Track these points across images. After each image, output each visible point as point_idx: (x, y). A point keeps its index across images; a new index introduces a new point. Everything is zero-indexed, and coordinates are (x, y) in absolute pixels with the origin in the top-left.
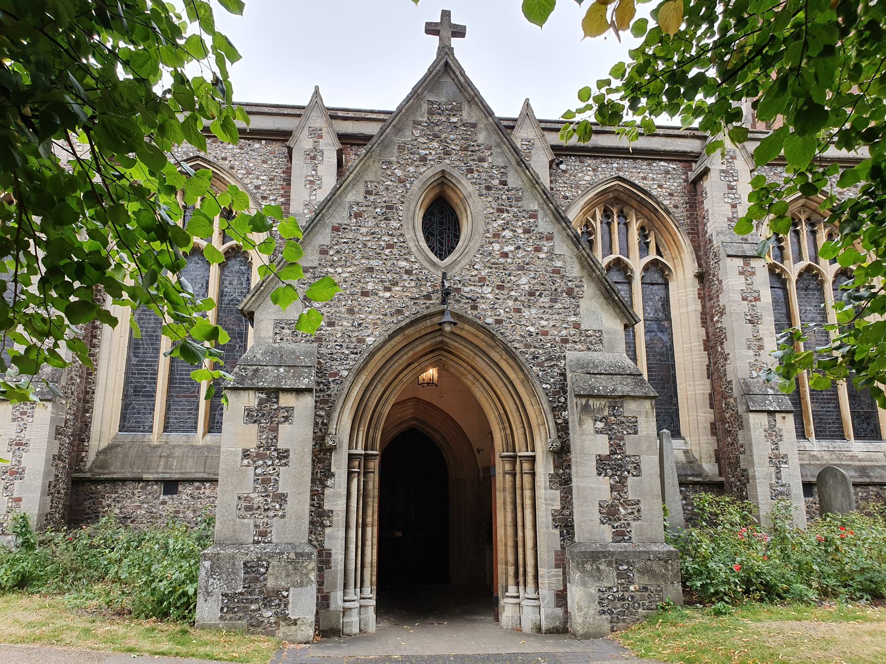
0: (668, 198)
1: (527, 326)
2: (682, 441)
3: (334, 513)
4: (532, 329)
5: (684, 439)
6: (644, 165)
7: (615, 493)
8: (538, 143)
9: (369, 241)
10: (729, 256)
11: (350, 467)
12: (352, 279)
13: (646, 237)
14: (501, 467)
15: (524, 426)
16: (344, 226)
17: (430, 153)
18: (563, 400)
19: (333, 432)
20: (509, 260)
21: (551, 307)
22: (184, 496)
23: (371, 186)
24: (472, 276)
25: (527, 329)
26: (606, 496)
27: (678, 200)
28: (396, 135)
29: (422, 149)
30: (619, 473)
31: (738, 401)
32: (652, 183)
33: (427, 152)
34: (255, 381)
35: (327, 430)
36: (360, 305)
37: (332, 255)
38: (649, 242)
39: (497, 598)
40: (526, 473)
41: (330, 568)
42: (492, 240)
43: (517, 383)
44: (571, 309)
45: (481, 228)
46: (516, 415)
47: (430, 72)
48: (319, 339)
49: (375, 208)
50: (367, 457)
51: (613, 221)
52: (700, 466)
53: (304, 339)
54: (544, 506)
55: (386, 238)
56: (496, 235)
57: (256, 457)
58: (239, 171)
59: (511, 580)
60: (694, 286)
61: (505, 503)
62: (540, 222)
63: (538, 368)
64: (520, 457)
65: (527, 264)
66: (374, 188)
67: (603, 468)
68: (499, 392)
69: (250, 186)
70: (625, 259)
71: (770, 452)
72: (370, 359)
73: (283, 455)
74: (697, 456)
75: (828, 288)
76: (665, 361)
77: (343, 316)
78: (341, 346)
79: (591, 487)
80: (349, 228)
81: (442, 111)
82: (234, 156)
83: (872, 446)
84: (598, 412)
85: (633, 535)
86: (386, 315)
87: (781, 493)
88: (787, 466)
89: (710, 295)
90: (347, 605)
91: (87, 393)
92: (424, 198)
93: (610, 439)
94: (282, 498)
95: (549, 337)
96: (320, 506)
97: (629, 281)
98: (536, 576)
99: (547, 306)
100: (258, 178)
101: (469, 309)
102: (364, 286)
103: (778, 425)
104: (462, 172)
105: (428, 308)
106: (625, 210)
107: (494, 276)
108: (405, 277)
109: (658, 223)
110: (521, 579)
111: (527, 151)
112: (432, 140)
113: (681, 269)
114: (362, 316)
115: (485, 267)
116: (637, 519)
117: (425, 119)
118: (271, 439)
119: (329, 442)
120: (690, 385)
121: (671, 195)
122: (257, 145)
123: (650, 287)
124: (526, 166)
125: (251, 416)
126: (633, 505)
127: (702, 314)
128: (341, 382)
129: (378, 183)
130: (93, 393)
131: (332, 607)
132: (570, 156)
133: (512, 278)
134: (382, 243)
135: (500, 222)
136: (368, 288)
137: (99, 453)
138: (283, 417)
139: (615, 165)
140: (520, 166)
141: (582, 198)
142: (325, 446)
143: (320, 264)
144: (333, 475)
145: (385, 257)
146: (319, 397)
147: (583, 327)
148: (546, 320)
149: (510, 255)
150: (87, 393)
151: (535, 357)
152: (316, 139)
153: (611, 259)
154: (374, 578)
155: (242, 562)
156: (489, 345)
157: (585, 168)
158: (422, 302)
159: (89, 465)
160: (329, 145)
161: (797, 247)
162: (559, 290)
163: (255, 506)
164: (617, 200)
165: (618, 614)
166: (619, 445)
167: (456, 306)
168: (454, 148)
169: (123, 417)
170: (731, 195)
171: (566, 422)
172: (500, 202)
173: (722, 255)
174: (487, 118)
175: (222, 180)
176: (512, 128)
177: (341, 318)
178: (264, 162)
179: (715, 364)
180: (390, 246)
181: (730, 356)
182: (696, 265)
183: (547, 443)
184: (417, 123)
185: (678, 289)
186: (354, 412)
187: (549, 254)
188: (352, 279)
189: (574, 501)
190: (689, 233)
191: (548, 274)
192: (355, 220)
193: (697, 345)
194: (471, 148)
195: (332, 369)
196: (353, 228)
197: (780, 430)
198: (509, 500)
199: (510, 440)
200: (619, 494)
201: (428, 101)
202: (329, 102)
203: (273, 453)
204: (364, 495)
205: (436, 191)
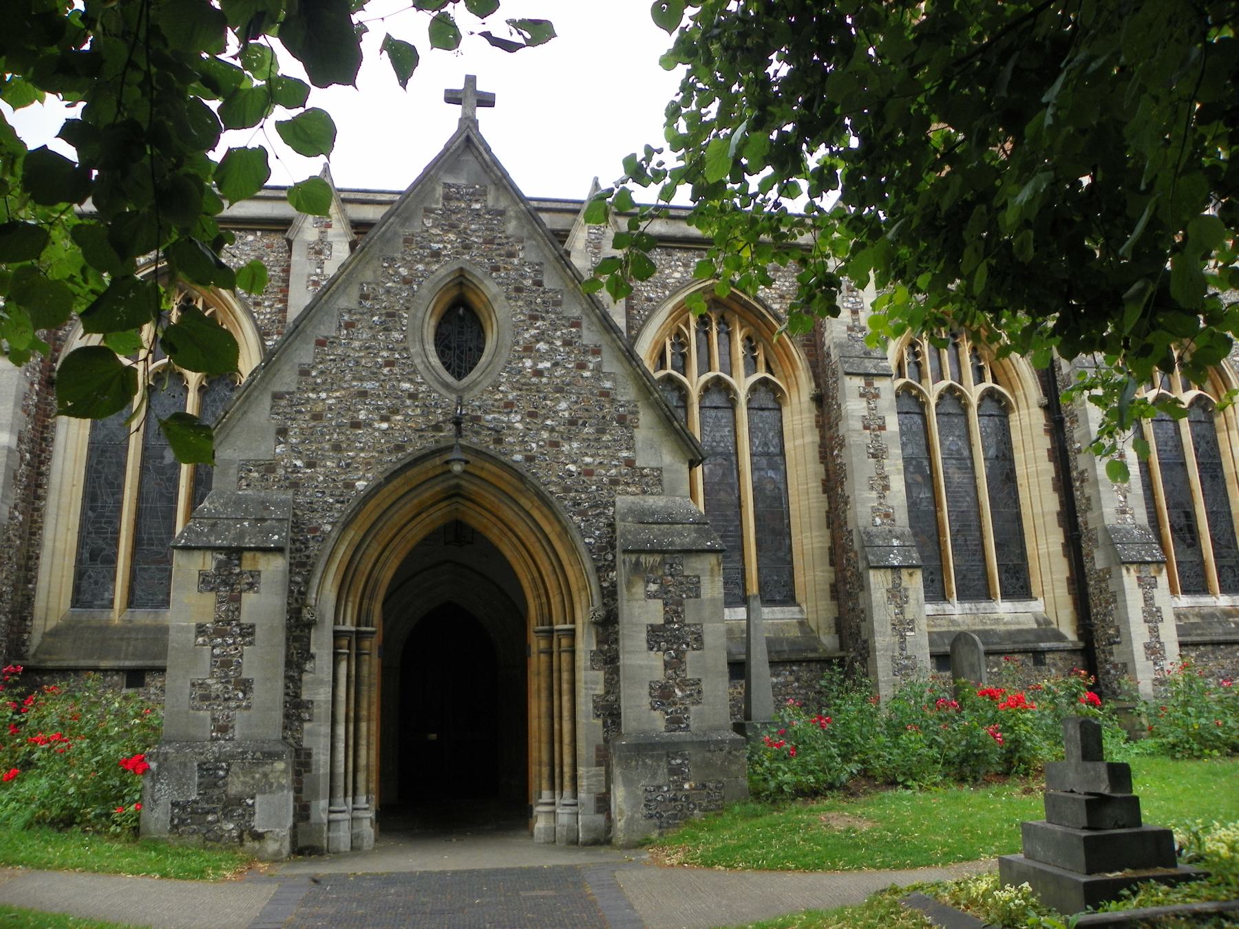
2: (796, 609)
4: (572, 467)
5: (799, 605)
7: (670, 672)
9: (362, 357)
10: (847, 374)
13: (753, 349)
14: (537, 644)
15: (561, 593)
17: (445, 248)
18: (610, 557)
20: (544, 380)
22: (152, 690)
24: (496, 400)
26: (659, 675)
28: (403, 225)
29: (435, 243)
30: (675, 647)
31: (859, 555)
33: (441, 246)
35: (304, 600)
37: (315, 377)
39: (531, 806)
41: (310, 771)
42: (522, 355)
43: (553, 537)
45: (508, 340)
46: (553, 577)
48: (295, 485)
50: (360, 636)
51: (711, 329)
52: (818, 639)
55: (385, 354)
56: (528, 349)
57: (214, 633)
59: (545, 784)
60: (810, 411)
62: (585, 332)
64: (558, 631)
65: (568, 385)
67: (656, 642)
68: (531, 548)
70: (727, 377)
71: (894, 617)
72: (360, 511)
74: (814, 627)
75: (973, 413)
77: (327, 454)
80: (337, 341)
83: (1020, 606)
85: (692, 722)
86: (382, 452)
87: (906, 667)
88: (913, 634)
89: (829, 423)
90: (333, 816)
91: (30, 558)
92: (437, 302)
93: (666, 605)
94: (245, 686)
95: (594, 478)
98: (574, 778)
102: (355, 415)
103: (903, 584)
105: (436, 442)
106: (726, 315)
108: (408, 402)
109: (766, 331)
110: (557, 781)
112: (448, 231)
113: (796, 389)
115: (513, 388)
120: (806, 537)
121: (782, 297)
122: (250, 238)
123: (760, 413)
125: (205, 582)
126: (693, 685)
127: (820, 446)
129: (378, 284)
130: (38, 558)
131: (313, 819)
133: (548, 402)
134: (379, 360)
135: (533, 332)
137: (45, 635)
138: (247, 584)
140: (560, 263)
143: (299, 388)
144: (312, 657)
145: (383, 377)
149: (546, 374)
150: (30, 558)
154: (373, 786)
155: (196, 764)
156: (517, 489)
159: (32, 650)
160: (340, 235)
161: (936, 363)
163: (213, 695)
165: (668, 817)
166: (676, 612)
167: (475, 440)
169: (77, 590)
170: (851, 299)
171: (614, 585)
172: (533, 307)
173: (840, 374)
177: (324, 458)
179: (836, 509)
180: (389, 363)
181: (851, 499)
182: (813, 385)
183: (588, 612)
184: (429, 211)
186: (342, 574)
187: (595, 372)
190: (804, 345)
193: (815, 486)
194: (498, 241)
195: (311, 523)
197: (906, 589)
198: (544, 685)
199: (546, 611)
204: (356, 682)
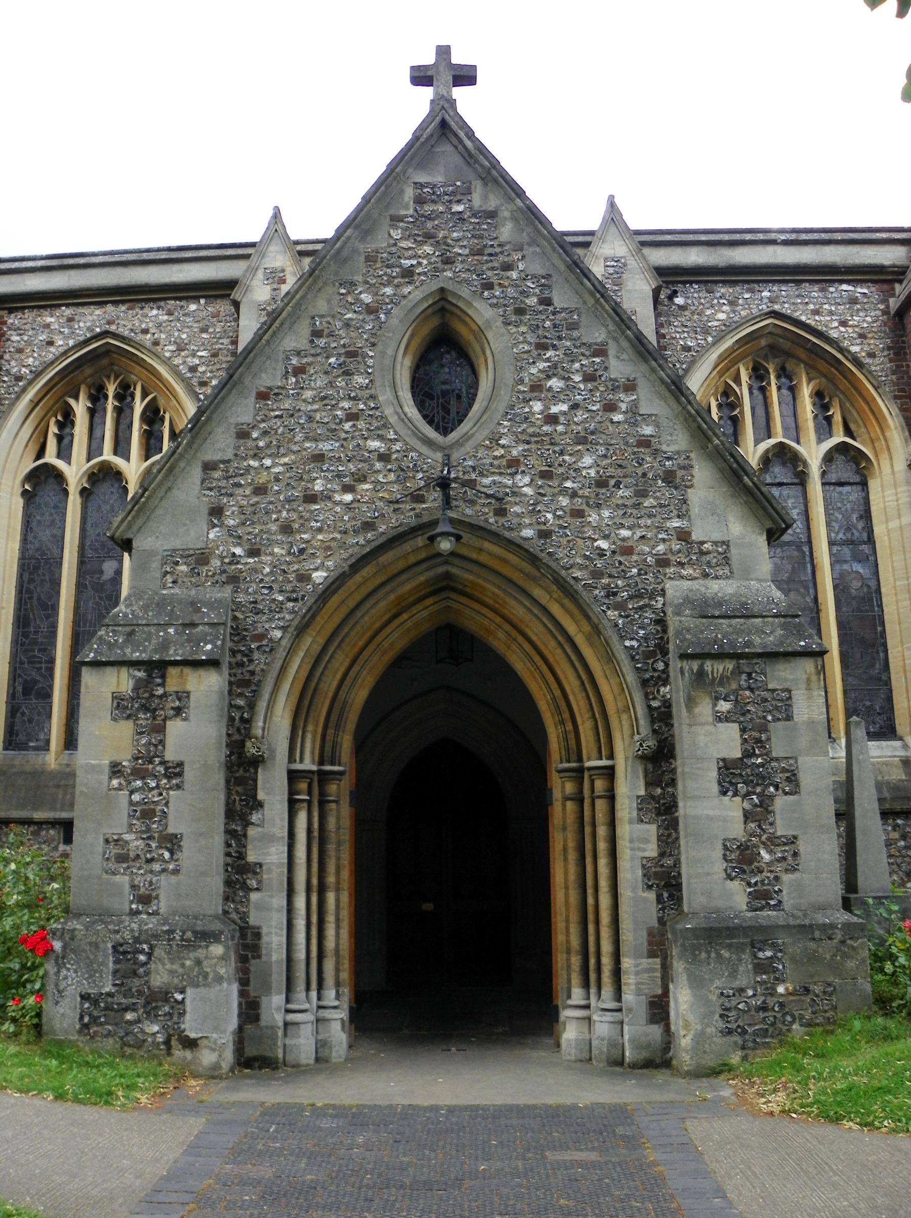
0: (858, 341)
1: (596, 540)
3: (264, 868)
4: (603, 544)
6: (815, 292)
7: (753, 825)
8: (632, 263)
9: (316, 411)
11: (292, 792)
12: (288, 475)
16: (276, 391)
17: (420, 264)
18: (660, 666)
19: (259, 732)
20: (560, 428)
21: (637, 506)
23: (321, 323)
24: (496, 458)
25: (596, 544)
26: (737, 830)
27: (877, 344)
28: (363, 240)
29: (406, 259)
30: (758, 790)
32: (829, 318)
33: (414, 262)
34: (128, 651)
35: (248, 730)
36: (301, 517)
37: (256, 439)
38: (832, 416)
40: (599, 797)
42: (528, 396)
43: (580, 640)
44: (672, 508)
45: (509, 376)
46: (581, 696)
47: (416, 137)
48: (234, 580)
49: (328, 357)
51: (769, 384)
53: (211, 580)
54: (628, 851)
55: (346, 404)
56: (536, 387)
57: (132, 774)
58: (166, 348)
61: (565, 850)
62: (613, 362)
63: (616, 613)
64: (590, 769)
65: (592, 433)
67: (731, 783)
69: (183, 369)
70: (793, 444)
72: (319, 609)
73: (175, 771)
76: (867, 611)
77: (274, 537)
78: (270, 588)
79: (708, 816)
80: (284, 392)
81: (439, 196)
82: (159, 325)
84: (721, 684)
86: (345, 533)
92: (412, 335)
94: (172, 842)
95: (635, 558)
96: (241, 856)
97: (802, 479)
99: (629, 503)
100: (194, 355)
101: (491, 514)
102: (309, 485)
104: (473, 289)
106: (788, 366)
107: (535, 456)
108: (378, 466)
109: (843, 383)
111: (616, 276)
114: (305, 536)
115: (518, 441)
116: (794, 869)
117: (411, 212)
118: (156, 746)
119: (251, 749)
121: (862, 336)
122: (193, 307)
124: (582, 271)
126: (785, 844)
128: (272, 650)
129: (333, 317)
132: (691, 283)
133: (567, 458)
134: (339, 413)
135: (542, 365)
136: (316, 488)
138: (173, 708)
139: (766, 294)
141: (713, 349)
142: (246, 757)
143: (236, 455)
144: (260, 805)
146: (235, 675)
147: (694, 537)
148: (629, 528)
149: (562, 419)
151: (611, 593)
152: (275, 286)
153: (769, 446)
156: (527, 576)
157: (715, 301)
158: (408, 507)
162: (650, 475)
164: (774, 350)
166: (758, 741)
167: (469, 511)
168: (460, 251)
171: (667, 703)
172: (540, 332)
174: (513, 200)
175: (142, 363)
176: (587, 245)
177: (271, 543)
178: (204, 330)
180: (352, 417)
184: (396, 220)
185: (883, 491)
187: (630, 415)
188: (288, 475)
189: (682, 842)
191: (630, 450)
192: (294, 380)
194: (490, 250)
195: (255, 629)
196: (291, 392)
198: (571, 844)
200: (760, 826)
201: (415, 183)
202: (296, 232)
203: (158, 768)
205: (435, 322)
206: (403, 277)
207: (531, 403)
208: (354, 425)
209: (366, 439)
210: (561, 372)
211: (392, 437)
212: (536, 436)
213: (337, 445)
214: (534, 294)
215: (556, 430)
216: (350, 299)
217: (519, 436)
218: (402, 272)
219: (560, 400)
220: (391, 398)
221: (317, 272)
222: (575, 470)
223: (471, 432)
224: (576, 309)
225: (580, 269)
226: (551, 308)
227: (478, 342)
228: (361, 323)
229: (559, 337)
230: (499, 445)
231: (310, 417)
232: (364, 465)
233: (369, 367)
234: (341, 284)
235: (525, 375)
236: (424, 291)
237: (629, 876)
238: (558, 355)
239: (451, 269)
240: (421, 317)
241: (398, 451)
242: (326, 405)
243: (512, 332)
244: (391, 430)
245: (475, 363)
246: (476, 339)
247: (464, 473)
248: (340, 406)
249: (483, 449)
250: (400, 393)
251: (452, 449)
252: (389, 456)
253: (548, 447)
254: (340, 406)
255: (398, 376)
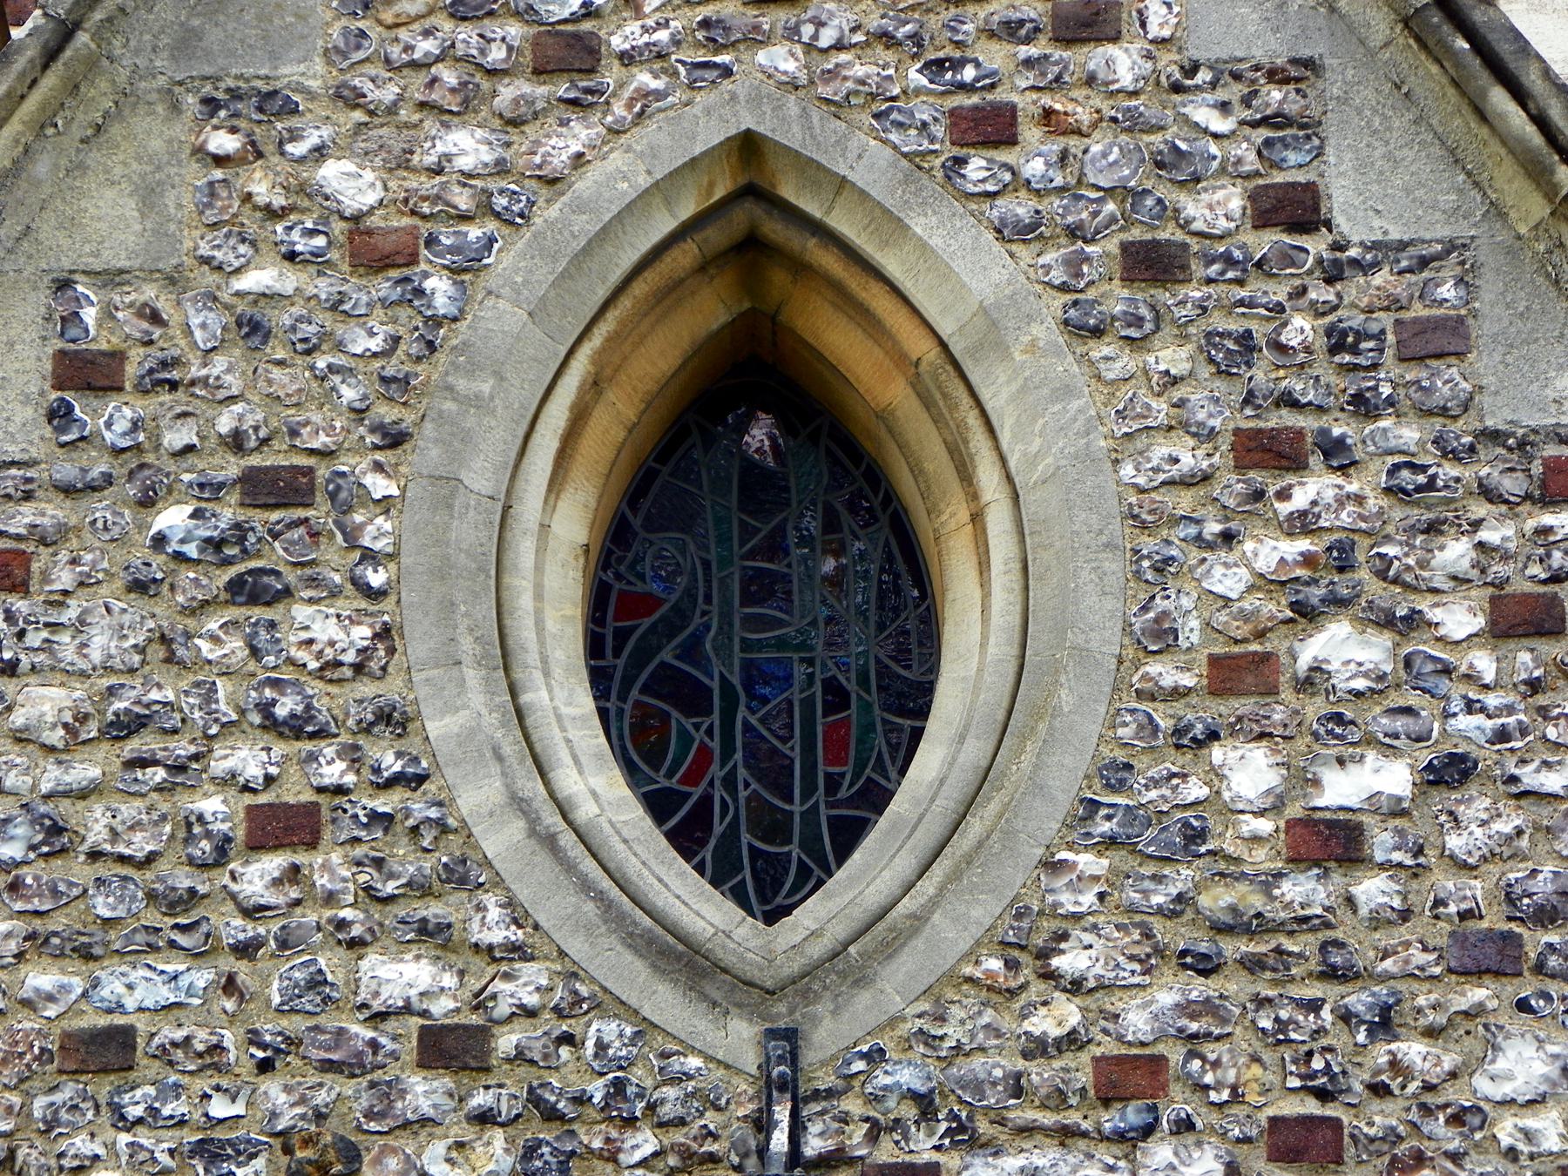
20: (1373, 890)
23: (108, 313)
24: (1038, 1048)
42: (1201, 714)
49: (148, 502)
66: (136, 327)
92: (595, 386)
104: (910, 141)
115: (1152, 959)
124: (1481, 48)
129: (173, 281)
133: (1413, 1050)
134: (211, 805)
149: (1381, 843)
172: (1261, 374)
206: (540, 72)
207: (1217, 753)
208: (293, 874)
209: (355, 944)
210: (1374, 588)
211: (497, 936)
212: (1250, 932)
213: (202, 978)
214: (1230, 171)
215: (1350, 901)
216: (262, 188)
217: (1157, 924)
218: (536, 42)
219: (1369, 741)
220: (491, 720)
221: (82, 38)
222: (1457, 1119)
223: (907, 905)
224: (1451, 246)
225: (1470, 34)
226: (1316, 245)
227: (938, 420)
228: (326, 319)
229: (1358, 399)
230: (1049, 976)
231: (56, 830)
232: (348, 1087)
233: (370, 557)
234: (211, 104)
235: (1182, 604)
236: (653, 152)
237: (528, 544)
238: (1359, 499)
239: (792, 33)
240: (639, 288)
241: (530, 1013)
242: (143, 763)
243: (1113, 372)
244: (490, 900)
245: (923, 526)
246: (927, 402)
247: (875, 1132)
248: (219, 767)
249: (972, 998)
250: (536, 696)
251: (808, 996)
252: (481, 1036)
253: (1313, 991)
254: (219, 767)
255: (523, 602)
